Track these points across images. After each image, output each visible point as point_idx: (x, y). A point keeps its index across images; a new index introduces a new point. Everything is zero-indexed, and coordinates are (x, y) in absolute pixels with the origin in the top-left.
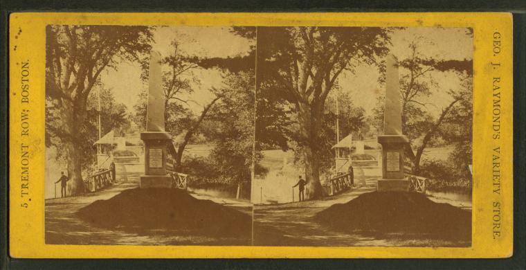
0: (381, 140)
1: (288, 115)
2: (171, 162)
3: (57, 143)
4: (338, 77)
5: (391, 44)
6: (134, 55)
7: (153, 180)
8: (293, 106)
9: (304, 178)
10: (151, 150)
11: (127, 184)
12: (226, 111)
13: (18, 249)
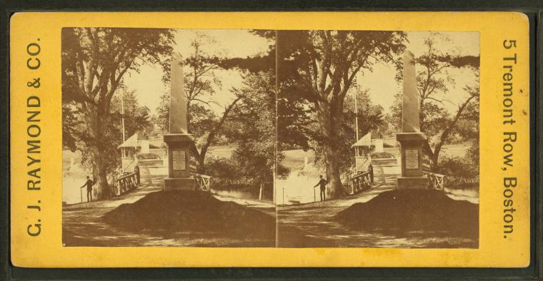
0: (399, 138)
1: (308, 115)
2: (194, 164)
3: (82, 147)
4: (356, 75)
5: (407, 41)
6: (156, 57)
7: (410, 182)
8: (312, 105)
9: (325, 177)
10: (407, 152)
11: (152, 187)
12: (247, 111)
13: (25, 253)
